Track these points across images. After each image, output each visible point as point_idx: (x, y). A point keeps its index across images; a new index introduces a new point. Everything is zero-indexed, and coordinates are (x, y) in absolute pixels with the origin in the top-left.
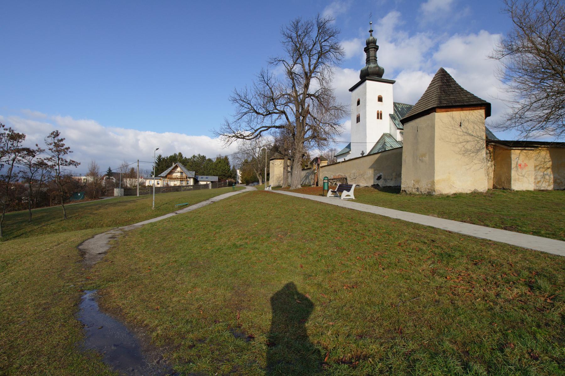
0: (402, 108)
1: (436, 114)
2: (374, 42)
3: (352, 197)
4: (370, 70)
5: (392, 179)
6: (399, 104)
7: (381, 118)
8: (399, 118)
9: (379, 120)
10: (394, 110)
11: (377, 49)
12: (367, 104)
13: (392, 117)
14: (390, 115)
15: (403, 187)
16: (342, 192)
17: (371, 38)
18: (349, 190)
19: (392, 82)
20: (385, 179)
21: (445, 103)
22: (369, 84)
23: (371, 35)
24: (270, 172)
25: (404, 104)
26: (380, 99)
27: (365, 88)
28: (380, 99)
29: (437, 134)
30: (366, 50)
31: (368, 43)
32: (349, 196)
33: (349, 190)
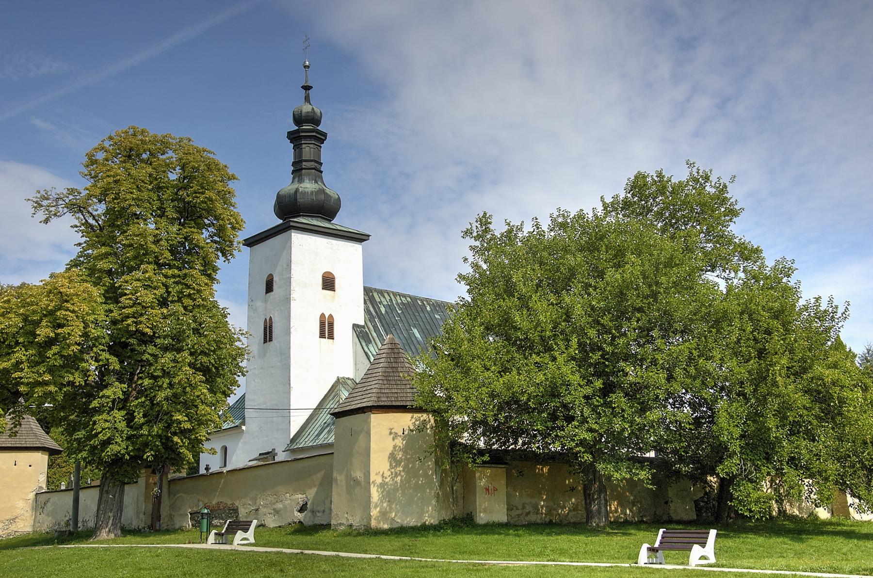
0: (390, 307)
2: (315, 120)
3: (252, 540)
4: (300, 200)
5: (324, 511)
6: (381, 292)
7: (331, 337)
8: (379, 335)
9: (325, 341)
10: (367, 311)
12: (293, 295)
13: (360, 333)
15: (333, 522)
17: (306, 108)
18: (246, 530)
19: (359, 238)
20: (313, 512)
23: (307, 99)
24: (816, 542)
25: (395, 294)
26: (329, 283)
27: (287, 247)
28: (329, 283)
29: (373, 446)
30: (295, 138)
31: (299, 119)
32: (247, 539)
33: (246, 530)
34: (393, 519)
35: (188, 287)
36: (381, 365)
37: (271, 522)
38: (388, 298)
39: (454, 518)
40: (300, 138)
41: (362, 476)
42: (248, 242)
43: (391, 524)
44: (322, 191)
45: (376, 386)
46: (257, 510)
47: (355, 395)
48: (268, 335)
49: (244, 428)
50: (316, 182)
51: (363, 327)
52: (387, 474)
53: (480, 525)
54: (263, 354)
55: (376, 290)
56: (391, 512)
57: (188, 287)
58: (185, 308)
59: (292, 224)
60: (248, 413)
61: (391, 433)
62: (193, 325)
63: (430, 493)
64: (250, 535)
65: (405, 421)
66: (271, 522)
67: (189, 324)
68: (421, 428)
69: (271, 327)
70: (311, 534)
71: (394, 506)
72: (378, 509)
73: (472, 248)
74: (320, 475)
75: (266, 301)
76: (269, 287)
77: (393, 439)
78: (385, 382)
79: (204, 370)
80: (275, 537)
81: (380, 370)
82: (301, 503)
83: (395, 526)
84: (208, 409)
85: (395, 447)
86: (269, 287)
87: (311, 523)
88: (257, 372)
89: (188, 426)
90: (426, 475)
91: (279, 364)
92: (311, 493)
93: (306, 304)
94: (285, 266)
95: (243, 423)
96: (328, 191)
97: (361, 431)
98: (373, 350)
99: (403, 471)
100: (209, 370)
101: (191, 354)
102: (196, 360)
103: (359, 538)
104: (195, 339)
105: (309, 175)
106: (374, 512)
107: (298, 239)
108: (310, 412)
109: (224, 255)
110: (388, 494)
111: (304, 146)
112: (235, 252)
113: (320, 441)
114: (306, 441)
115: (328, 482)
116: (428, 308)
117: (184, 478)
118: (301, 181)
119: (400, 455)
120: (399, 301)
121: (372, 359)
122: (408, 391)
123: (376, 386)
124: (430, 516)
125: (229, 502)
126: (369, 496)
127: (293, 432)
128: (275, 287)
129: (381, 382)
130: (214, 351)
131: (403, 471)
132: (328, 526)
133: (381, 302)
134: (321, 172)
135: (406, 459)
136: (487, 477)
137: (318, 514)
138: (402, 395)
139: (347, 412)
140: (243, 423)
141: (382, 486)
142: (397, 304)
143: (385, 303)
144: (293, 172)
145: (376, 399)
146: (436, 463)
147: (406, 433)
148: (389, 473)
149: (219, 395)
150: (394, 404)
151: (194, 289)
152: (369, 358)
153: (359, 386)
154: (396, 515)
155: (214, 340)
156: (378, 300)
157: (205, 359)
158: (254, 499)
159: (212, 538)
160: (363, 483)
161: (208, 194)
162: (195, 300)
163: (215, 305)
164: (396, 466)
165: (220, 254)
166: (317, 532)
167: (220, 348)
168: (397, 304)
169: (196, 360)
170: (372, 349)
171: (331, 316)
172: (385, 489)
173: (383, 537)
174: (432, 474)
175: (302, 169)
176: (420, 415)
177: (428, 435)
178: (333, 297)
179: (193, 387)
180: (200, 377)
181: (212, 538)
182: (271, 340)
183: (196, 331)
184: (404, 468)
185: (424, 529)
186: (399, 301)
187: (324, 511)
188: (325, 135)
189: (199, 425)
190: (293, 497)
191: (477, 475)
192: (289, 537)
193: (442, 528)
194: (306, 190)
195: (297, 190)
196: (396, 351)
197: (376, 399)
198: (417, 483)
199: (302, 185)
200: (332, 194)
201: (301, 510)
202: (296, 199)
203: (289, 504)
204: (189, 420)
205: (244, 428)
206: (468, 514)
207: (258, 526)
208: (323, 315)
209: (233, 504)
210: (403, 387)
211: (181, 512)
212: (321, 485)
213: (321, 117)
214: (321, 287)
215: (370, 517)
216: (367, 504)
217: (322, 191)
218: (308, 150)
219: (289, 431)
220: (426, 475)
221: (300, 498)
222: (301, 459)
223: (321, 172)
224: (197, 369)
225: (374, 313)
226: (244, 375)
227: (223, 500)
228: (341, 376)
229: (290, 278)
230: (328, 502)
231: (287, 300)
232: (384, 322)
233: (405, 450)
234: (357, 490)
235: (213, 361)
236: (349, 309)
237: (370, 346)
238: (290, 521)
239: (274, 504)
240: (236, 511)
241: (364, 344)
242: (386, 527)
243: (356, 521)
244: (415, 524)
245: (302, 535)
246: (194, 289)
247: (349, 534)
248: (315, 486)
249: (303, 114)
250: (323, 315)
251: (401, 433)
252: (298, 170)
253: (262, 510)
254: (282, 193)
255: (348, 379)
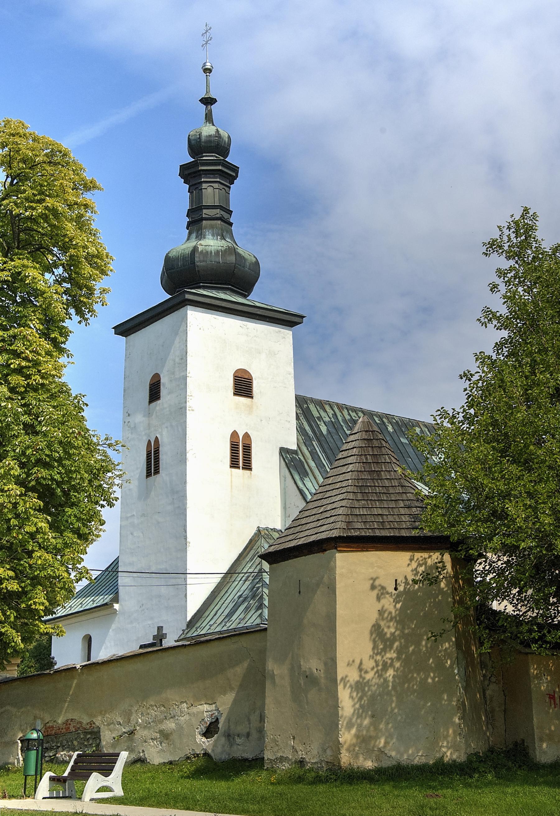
1: (338, 555)
3: (119, 791)
5: (248, 735)
6: (320, 404)
7: (248, 466)
8: (320, 465)
9: (239, 472)
10: (301, 430)
11: (232, 179)
12: (190, 403)
13: (290, 460)
14: (283, 451)
15: (268, 755)
16: (87, 778)
17: (208, 130)
18: (107, 772)
20: (228, 736)
21: (359, 529)
22: (201, 326)
23: (209, 118)
25: (341, 407)
26: (243, 386)
27: (181, 330)
28: (243, 386)
29: (340, 611)
30: (189, 174)
31: (197, 147)
33: (107, 772)
34: (381, 751)
35: (17, 355)
36: (351, 467)
37: (156, 755)
38: (331, 412)
39: (491, 750)
40: (199, 174)
41: (321, 667)
42: (122, 329)
43: (378, 759)
44: (232, 251)
45: (344, 503)
46: (132, 733)
47: (303, 521)
48: (153, 464)
49: (116, 606)
50: (223, 238)
51: (295, 452)
52: (369, 664)
53: (544, 766)
54: (145, 494)
55: (312, 400)
56: (377, 738)
57: (17, 355)
58: (12, 390)
59: (188, 296)
60: (123, 580)
61: (373, 587)
62: (25, 418)
63: (451, 700)
64: (115, 780)
65: (399, 566)
66: (156, 755)
67: (16, 415)
68: (430, 579)
69: (157, 451)
70: (226, 778)
71: (382, 726)
72: (354, 731)
73: (501, 273)
74: (240, 670)
75: (149, 415)
76: (155, 393)
77: (379, 598)
78: (359, 497)
79: (45, 492)
80: (162, 785)
81: (348, 476)
82: (208, 720)
83: (386, 763)
84: (49, 557)
85: (381, 612)
86: (155, 393)
87: (224, 757)
88: (136, 521)
89: (14, 586)
90: (440, 666)
91: (169, 508)
92: (226, 701)
93: (208, 417)
94: (177, 360)
95: (116, 599)
96: (240, 251)
97: (318, 585)
98: (310, 486)
99: (398, 658)
100: (52, 493)
101: (22, 465)
102: (28, 475)
103: (321, 788)
104: (27, 440)
105: (212, 227)
106: (346, 737)
107: (195, 317)
108: (217, 579)
109: (79, 312)
110: (372, 703)
111: (204, 186)
112: (96, 307)
113: (233, 624)
114: (211, 626)
115: (255, 683)
116: (390, 428)
117: (14, 680)
118: (200, 236)
119: (390, 630)
120: (348, 417)
121: (309, 497)
122: (402, 511)
123: (344, 503)
124: (455, 747)
125: (85, 720)
126: (336, 705)
127: (191, 612)
128: (163, 392)
129: (351, 496)
130: (60, 460)
131: (398, 658)
132: (256, 763)
133: (320, 418)
134: (231, 224)
135: (403, 635)
136: (550, 672)
137: (238, 741)
138: (390, 518)
139: (287, 557)
140: (116, 599)
141: (360, 686)
142: (345, 420)
143: (327, 419)
144: (189, 225)
145: (344, 525)
146: (458, 645)
147: (401, 588)
148: (372, 663)
149: (68, 534)
150: (378, 533)
151: (26, 359)
152: (304, 498)
153: (311, 506)
154: (386, 743)
155: (60, 443)
156: (316, 414)
157: (44, 473)
158: (128, 715)
159: (44, 785)
160: (323, 681)
161: (49, 202)
162: (28, 377)
163: (64, 390)
164: (384, 650)
165: (72, 311)
166: (237, 773)
167: (70, 455)
168: (345, 420)
169: (28, 475)
170: (309, 485)
171: (247, 436)
172: (364, 694)
173: (367, 786)
174: (451, 666)
175: (202, 219)
176: (426, 555)
177: (441, 590)
178: (250, 408)
179: (23, 519)
180: (35, 501)
181: (44, 785)
182: (157, 472)
183: (30, 429)
184: (399, 652)
185: (437, 773)
186: (348, 417)
187: (248, 735)
188: (235, 169)
189: (34, 586)
190: (194, 710)
191: (533, 671)
192: (188, 783)
193: (475, 770)
194: (209, 249)
195: (195, 249)
196: (376, 443)
197: (344, 525)
198: (423, 682)
199: (202, 242)
200: (246, 256)
201: (208, 733)
202: (193, 262)
203: (186, 722)
204: (16, 577)
205: (116, 606)
206: (516, 744)
207: (130, 764)
208: (234, 434)
209: (91, 723)
210: (392, 505)
211: (7, 739)
212: (242, 687)
213: (229, 144)
214: (231, 390)
215: (337, 746)
216: (331, 723)
217: (232, 251)
218: (210, 193)
219: (184, 608)
220: (440, 665)
221: (205, 710)
222: (210, 640)
223: (231, 224)
224: (28, 489)
225: (310, 433)
226: (111, 505)
227: (76, 716)
228: (263, 526)
229: (185, 378)
230: (254, 718)
231: (181, 410)
232: (326, 446)
233: (401, 619)
234: (313, 694)
235: (57, 477)
236: (274, 425)
237: (307, 480)
238: (188, 752)
239: (161, 722)
240: (96, 735)
241: (297, 477)
242: (369, 764)
243: (312, 754)
244: (424, 760)
245: (210, 778)
246: (26, 359)
247: (300, 780)
248: (232, 689)
249: (203, 139)
250: (234, 434)
251: (391, 589)
252: (196, 221)
253: (141, 733)
254: (173, 254)
255: (274, 530)
